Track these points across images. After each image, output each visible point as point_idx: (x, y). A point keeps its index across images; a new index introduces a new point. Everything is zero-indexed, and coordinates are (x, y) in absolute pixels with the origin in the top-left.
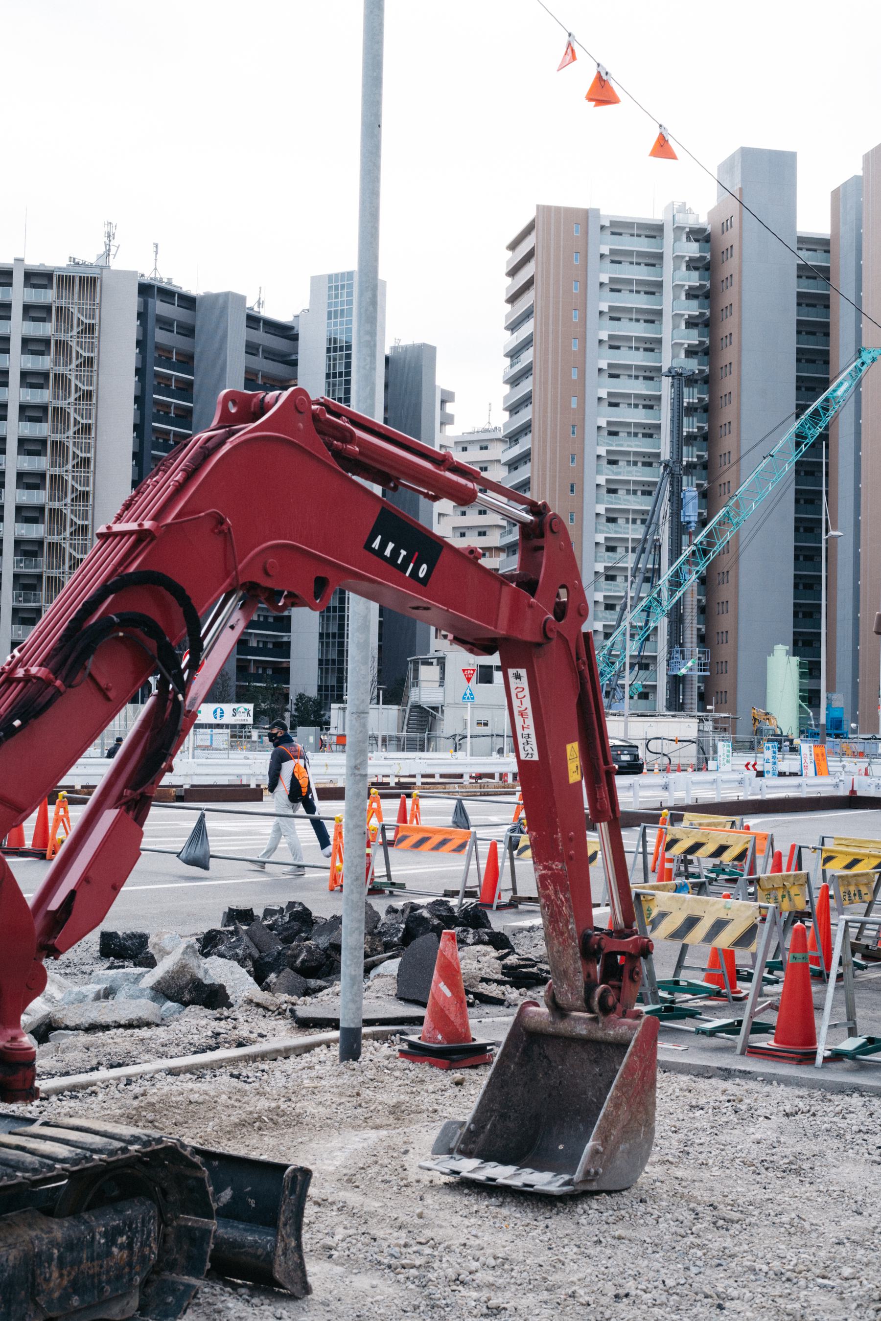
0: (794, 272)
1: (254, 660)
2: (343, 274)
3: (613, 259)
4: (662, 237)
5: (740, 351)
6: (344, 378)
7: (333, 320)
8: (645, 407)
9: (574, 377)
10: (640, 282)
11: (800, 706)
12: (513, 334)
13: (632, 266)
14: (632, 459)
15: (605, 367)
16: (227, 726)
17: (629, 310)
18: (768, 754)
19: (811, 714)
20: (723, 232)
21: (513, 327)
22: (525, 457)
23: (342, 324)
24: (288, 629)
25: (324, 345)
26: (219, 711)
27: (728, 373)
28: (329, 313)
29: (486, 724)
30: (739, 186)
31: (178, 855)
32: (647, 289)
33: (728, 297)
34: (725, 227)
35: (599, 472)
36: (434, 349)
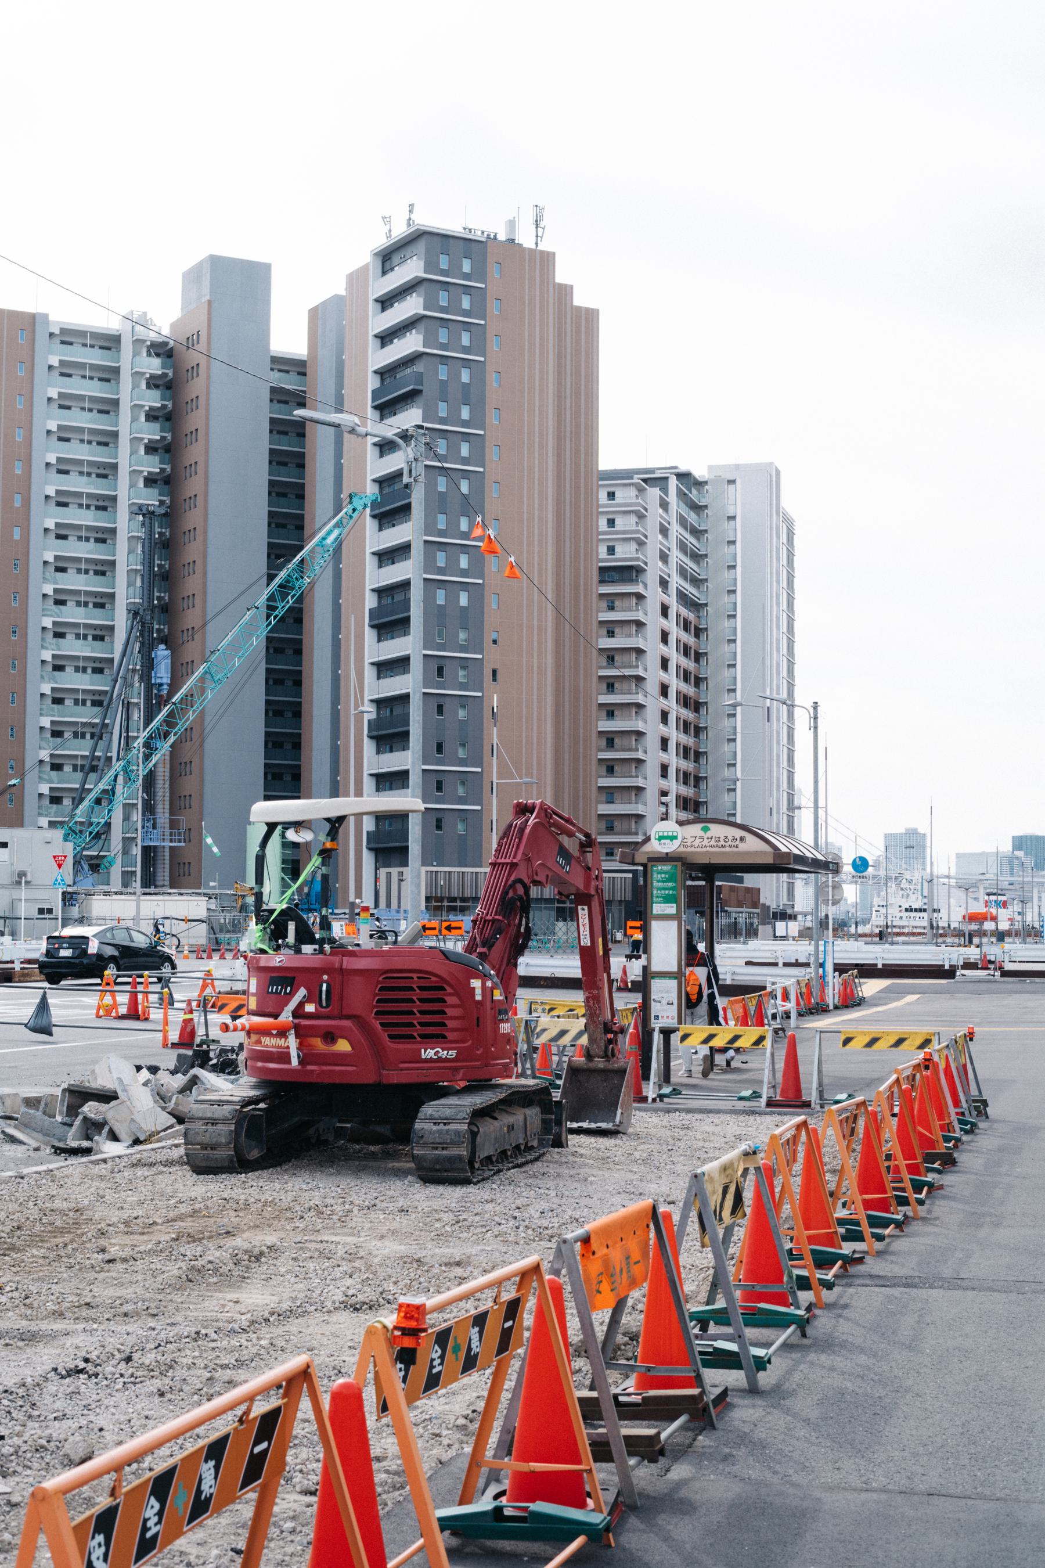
0: (267, 395)
3: (64, 339)
4: (114, 538)
5: (206, 484)
8: (97, 540)
10: (93, 367)
13: (83, 380)
14: (82, 599)
15: (53, 494)
17: (81, 398)
27: (192, 539)
30: (208, 298)
32: (101, 407)
33: (194, 420)
34: (191, 342)
35: (41, 780)
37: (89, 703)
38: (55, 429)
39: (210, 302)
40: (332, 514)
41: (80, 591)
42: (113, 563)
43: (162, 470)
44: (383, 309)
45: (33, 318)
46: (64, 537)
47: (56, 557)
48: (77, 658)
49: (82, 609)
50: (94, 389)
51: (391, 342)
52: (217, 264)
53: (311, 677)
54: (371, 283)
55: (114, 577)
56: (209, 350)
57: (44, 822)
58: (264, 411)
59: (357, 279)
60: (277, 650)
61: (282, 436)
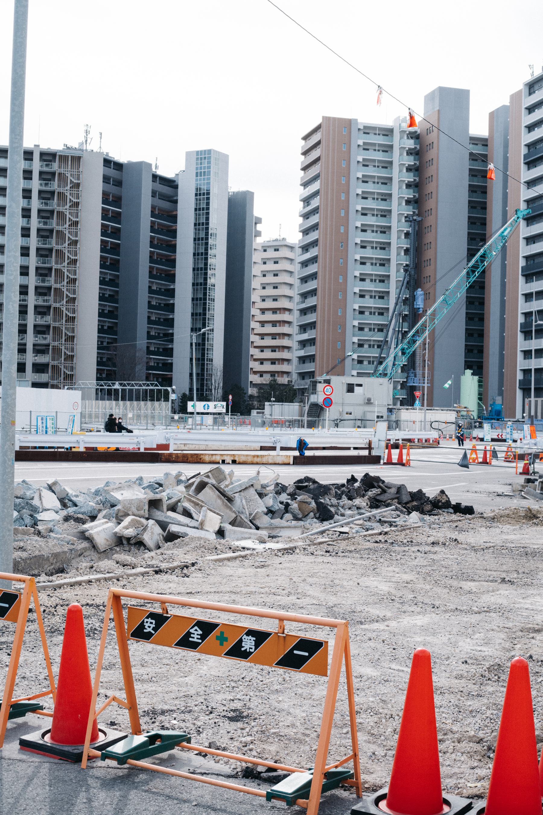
0: (467, 156)
1: (153, 374)
2: (205, 151)
4: (392, 136)
6: (205, 211)
7: (199, 178)
9: (343, 215)
11: (479, 403)
12: (305, 189)
13: (375, 136)
16: (211, 414)
18: (508, 430)
19: (484, 408)
20: (427, 134)
21: (305, 185)
22: (314, 260)
23: (204, 179)
24: (171, 356)
25: (194, 192)
26: (206, 406)
28: (197, 173)
29: (351, 414)
30: (438, 108)
31: (458, 464)
33: (430, 171)
34: (429, 131)
36: (252, 194)
37: (378, 248)
38: (362, 144)
39: (439, 111)
40: (501, 225)
41: (375, 160)
42: (389, 244)
43: (415, 180)
44: (530, 113)
45: (350, 121)
46: (365, 214)
47: (362, 241)
48: (371, 291)
49: (372, 300)
50: (379, 156)
51: (534, 111)
52: (442, 90)
53: (489, 301)
54: (523, 118)
55: (389, 283)
56: (438, 125)
57: (354, 373)
58: (466, 165)
59: (515, 98)
60: (472, 207)
61: (474, 178)
